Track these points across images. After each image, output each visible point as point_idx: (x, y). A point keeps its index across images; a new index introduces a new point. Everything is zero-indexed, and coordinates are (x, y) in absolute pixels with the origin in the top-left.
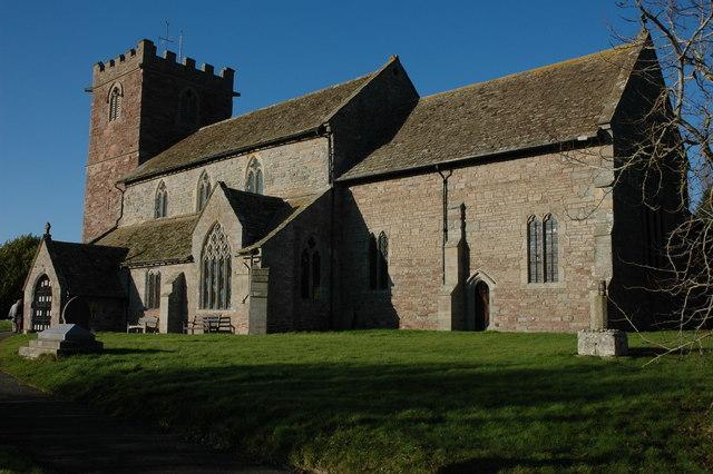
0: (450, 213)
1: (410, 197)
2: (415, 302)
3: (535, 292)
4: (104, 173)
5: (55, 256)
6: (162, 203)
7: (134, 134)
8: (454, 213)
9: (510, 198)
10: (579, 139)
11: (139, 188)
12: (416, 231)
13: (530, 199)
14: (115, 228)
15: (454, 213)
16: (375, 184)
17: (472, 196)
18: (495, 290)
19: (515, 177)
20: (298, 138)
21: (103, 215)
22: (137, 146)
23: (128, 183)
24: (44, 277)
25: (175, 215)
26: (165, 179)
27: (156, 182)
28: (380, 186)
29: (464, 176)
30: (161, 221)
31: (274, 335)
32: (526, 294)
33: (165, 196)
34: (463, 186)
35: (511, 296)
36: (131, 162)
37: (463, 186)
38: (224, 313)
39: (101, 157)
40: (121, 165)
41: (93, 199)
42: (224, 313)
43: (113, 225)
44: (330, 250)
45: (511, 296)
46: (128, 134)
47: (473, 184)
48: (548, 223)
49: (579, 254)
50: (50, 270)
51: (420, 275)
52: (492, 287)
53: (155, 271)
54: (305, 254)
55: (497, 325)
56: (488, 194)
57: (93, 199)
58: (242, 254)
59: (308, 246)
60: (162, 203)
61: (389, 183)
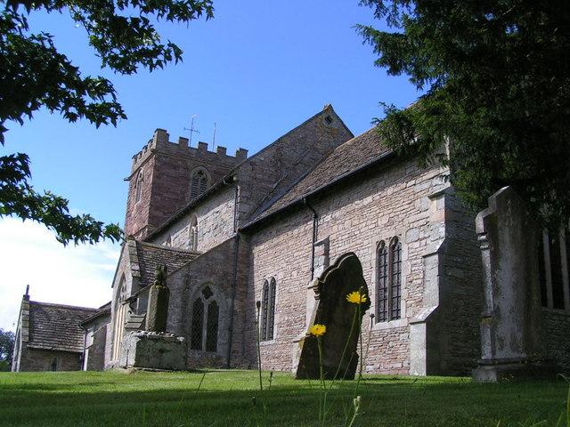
12: (295, 273)
44: (230, 300)
54: (198, 304)
59: (201, 295)
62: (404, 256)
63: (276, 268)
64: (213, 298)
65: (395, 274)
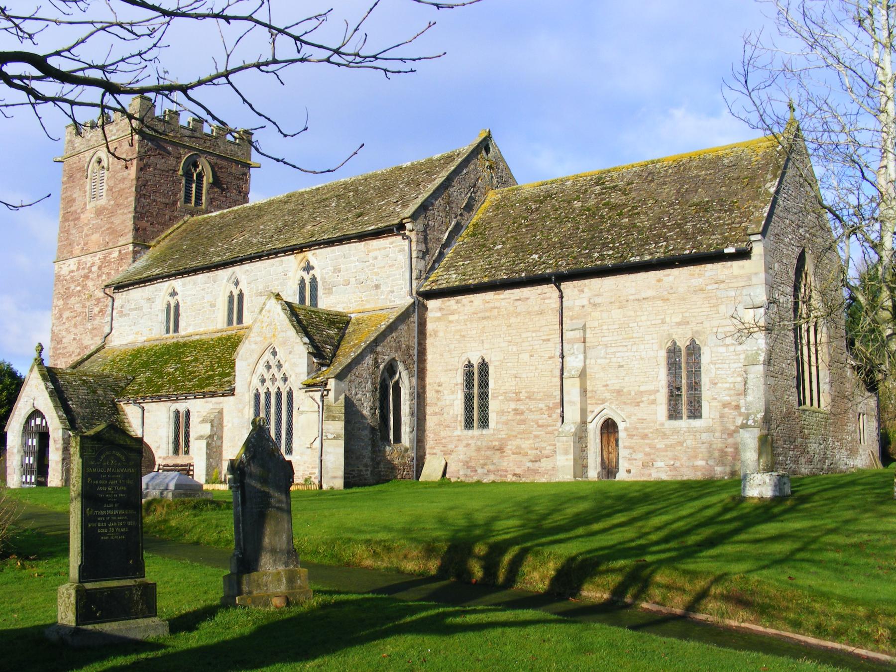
0: (568, 335)
1: (518, 314)
2: (526, 444)
3: (676, 432)
4: (82, 272)
5: (354, 409)
6: (174, 315)
7: (125, 219)
8: (409, 65)
9: (644, 318)
10: (726, 251)
11: (137, 294)
12: (525, 357)
13: (668, 320)
14: (103, 347)
15: (409, 65)
16: (471, 297)
17: (596, 314)
18: (626, 429)
19: (650, 293)
20: (362, 237)
21: (80, 329)
22: (129, 238)
23: (120, 287)
24: (36, 413)
25: (190, 330)
26: (177, 284)
27: (165, 287)
28: (478, 299)
29: (586, 290)
30: (171, 338)
31: (354, 490)
32: (665, 434)
33: (177, 306)
34: (585, 302)
35: (645, 436)
36: (121, 258)
37: (585, 302)
38: (685, 417)
39: (77, 250)
40: (105, 261)
41: (66, 307)
42: (685, 417)
43: (98, 341)
45: (645, 436)
46: (117, 221)
47: (598, 300)
48: (694, 350)
49: (727, 385)
50: (46, 404)
51: (531, 411)
52: (621, 426)
53: (182, 406)
55: (629, 471)
56: (616, 313)
57: (66, 307)
58: (308, 386)
60: (174, 315)
61: (490, 296)
62: (705, 359)
63: (486, 346)
64: (283, 370)
65: (695, 372)
